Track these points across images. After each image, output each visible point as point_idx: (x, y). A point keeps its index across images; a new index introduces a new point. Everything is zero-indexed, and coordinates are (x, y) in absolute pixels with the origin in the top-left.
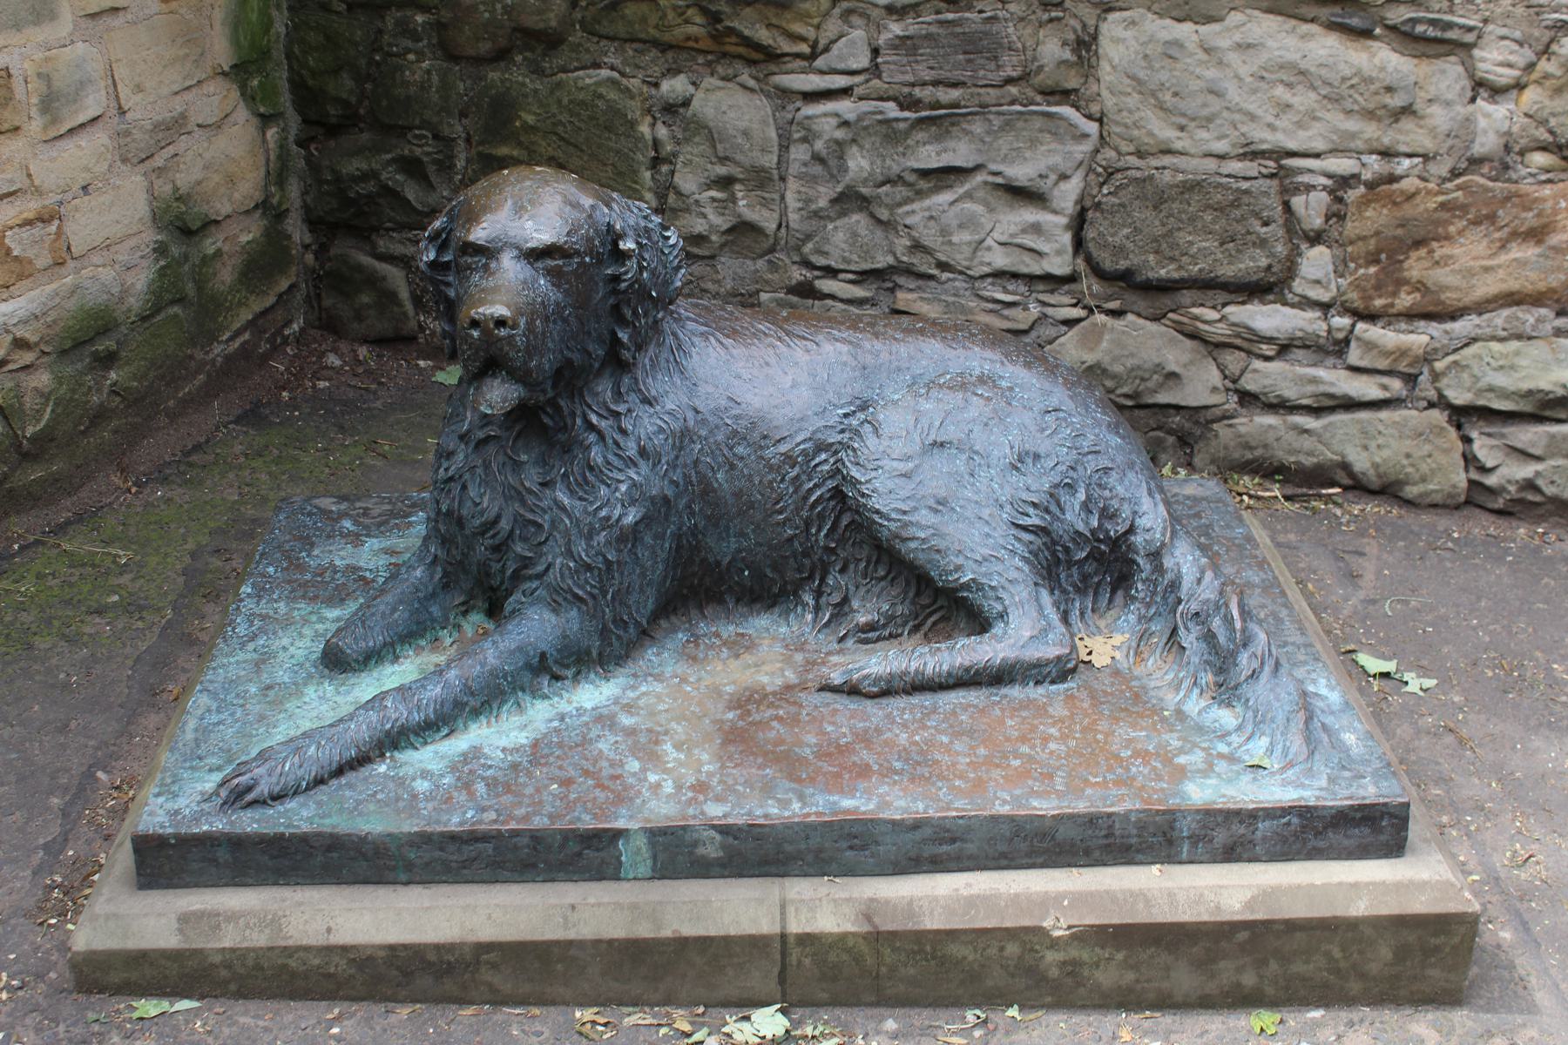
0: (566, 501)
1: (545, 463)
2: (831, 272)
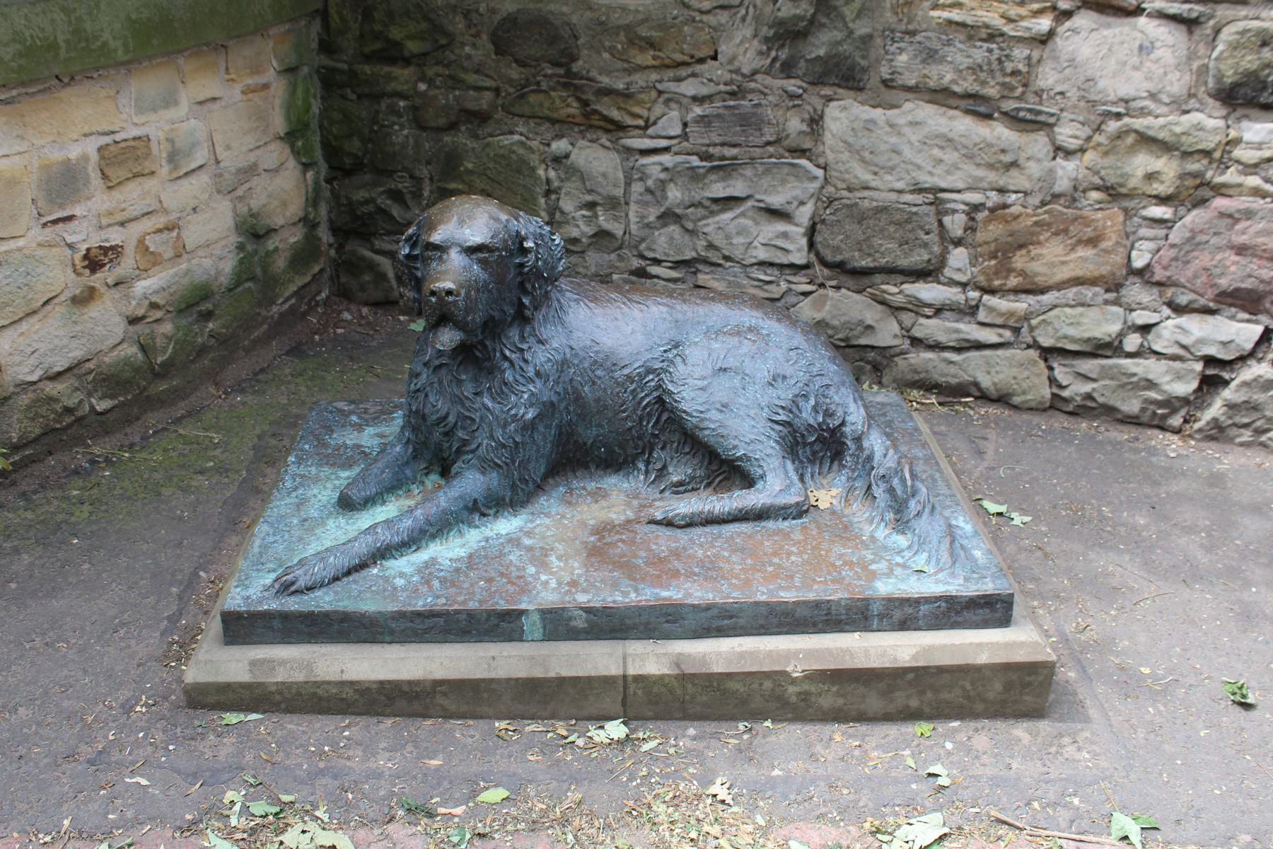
0: (490, 405)
2: (657, 262)
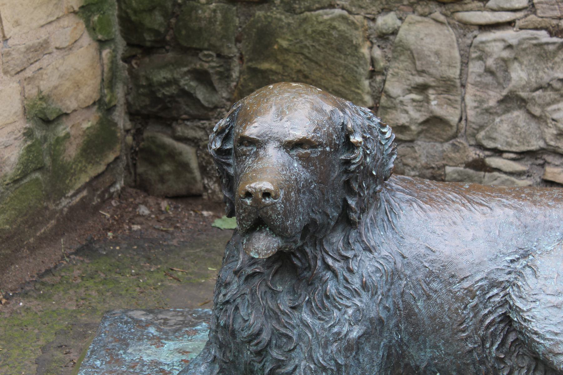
0: (309, 320)
1: (295, 293)
2: (498, 152)
